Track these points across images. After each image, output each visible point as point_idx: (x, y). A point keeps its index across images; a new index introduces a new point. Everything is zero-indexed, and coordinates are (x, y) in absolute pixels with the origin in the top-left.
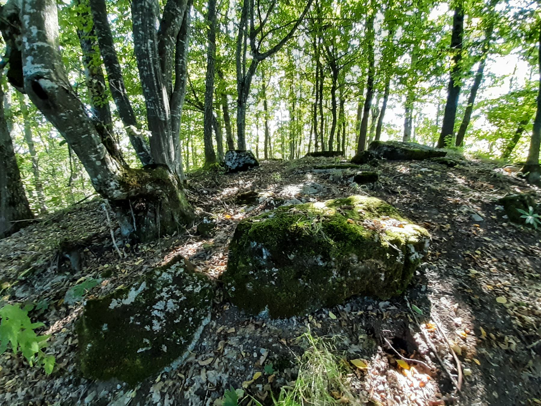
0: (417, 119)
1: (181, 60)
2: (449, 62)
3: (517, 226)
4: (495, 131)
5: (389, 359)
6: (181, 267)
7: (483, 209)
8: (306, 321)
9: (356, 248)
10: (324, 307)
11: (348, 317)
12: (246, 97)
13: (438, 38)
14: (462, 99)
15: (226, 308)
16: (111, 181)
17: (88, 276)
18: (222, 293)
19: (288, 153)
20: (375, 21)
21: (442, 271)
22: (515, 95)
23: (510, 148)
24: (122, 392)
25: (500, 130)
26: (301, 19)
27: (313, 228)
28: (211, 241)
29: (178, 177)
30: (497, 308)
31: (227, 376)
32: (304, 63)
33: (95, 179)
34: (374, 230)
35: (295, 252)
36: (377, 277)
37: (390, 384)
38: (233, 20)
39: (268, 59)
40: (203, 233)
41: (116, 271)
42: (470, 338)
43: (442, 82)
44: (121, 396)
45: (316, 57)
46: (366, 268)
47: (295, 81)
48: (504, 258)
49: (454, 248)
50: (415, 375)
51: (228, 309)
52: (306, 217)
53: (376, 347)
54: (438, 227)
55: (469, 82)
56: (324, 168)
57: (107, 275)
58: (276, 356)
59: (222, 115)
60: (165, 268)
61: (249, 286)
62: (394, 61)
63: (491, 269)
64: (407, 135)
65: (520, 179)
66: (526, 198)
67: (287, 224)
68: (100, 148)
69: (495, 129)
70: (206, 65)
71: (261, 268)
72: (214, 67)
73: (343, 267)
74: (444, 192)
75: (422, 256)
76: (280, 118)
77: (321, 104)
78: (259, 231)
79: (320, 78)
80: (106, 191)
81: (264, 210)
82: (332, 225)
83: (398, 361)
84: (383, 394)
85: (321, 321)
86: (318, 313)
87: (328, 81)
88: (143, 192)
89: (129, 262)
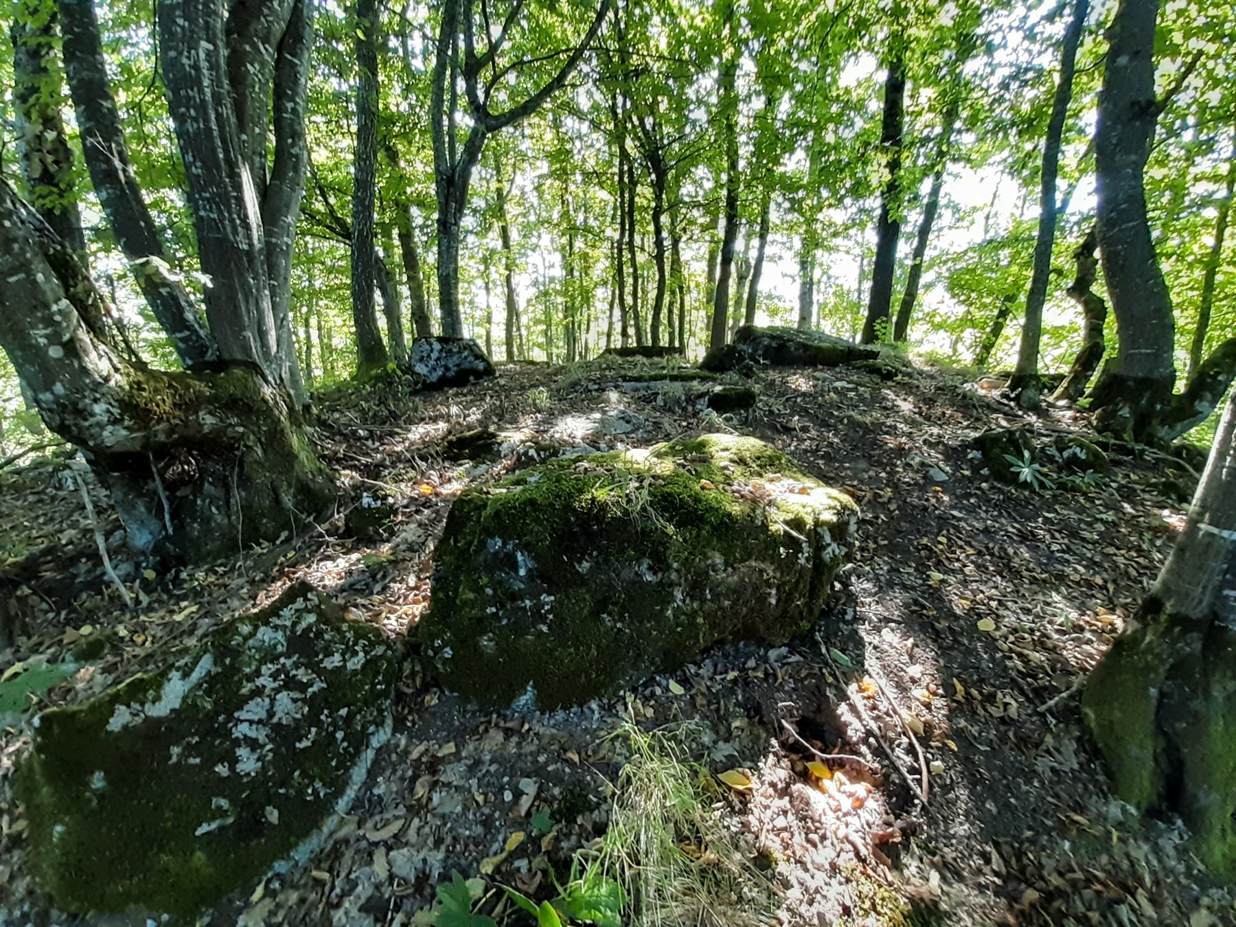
0: (822, 286)
1: (290, 105)
2: (877, 173)
4: (960, 315)
5: (793, 763)
7: (947, 459)
8: (620, 707)
9: (719, 539)
10: (658, 672)
11: (708, 688)
12: (460, 211)
13: (859, 123)
14: (903, 249)
15: (432, 700)
16: (96, 401)
17: (33, 659)
18: (417, 668)
19: (560, 349)
20: (738, 72)
22: (993, 245)
23: (987, 348)
25: (969, 312)
26: (584, 46)
27: (629, 501)
28: (386, 548)
29: (289, 395)
31: (441, 855)
32: (592, 149)
35: (591, 555)
36: (763, 598)
37: (797, 813)
38: (422, 27)
39: (507, 130)
40: (365, 527)
41: (116, 644)
42: (938, 702)
43: (868, 212)
45: (617, 137)
46: (742, 580)
47: (572, 188)
48: (987, 548)
49: (899, 533)
51: (435, 701)
52: (613, 478)
53: (767, 741)
54: (869, 495)
55: (914, 217)
57: (89, 653)
58: (556, 791)
59: (398, 251)
60: (264, 618)
61: (486, 642)
62: (776, 161)
63: (967, 570)
64: (804, 318)
67: (570, 495)
68: (60, 312)
69: (961, 310)
70: (354, 129)
71: (515, 597)
72: (375, 136)
73: (695, 581)
74: (877, 427)
75: (844, 550)
76: (541, 271)
77: (631, 243)
78: (507, 514)
79: (627, 186)
80: (80, 428)
81: (513, 471)
82: (670, 494)
83: (809, 764)
84: (785, 835)
86: (645, 685)
87: (644, 194)
88: (192, 432)
89: (155, 617)
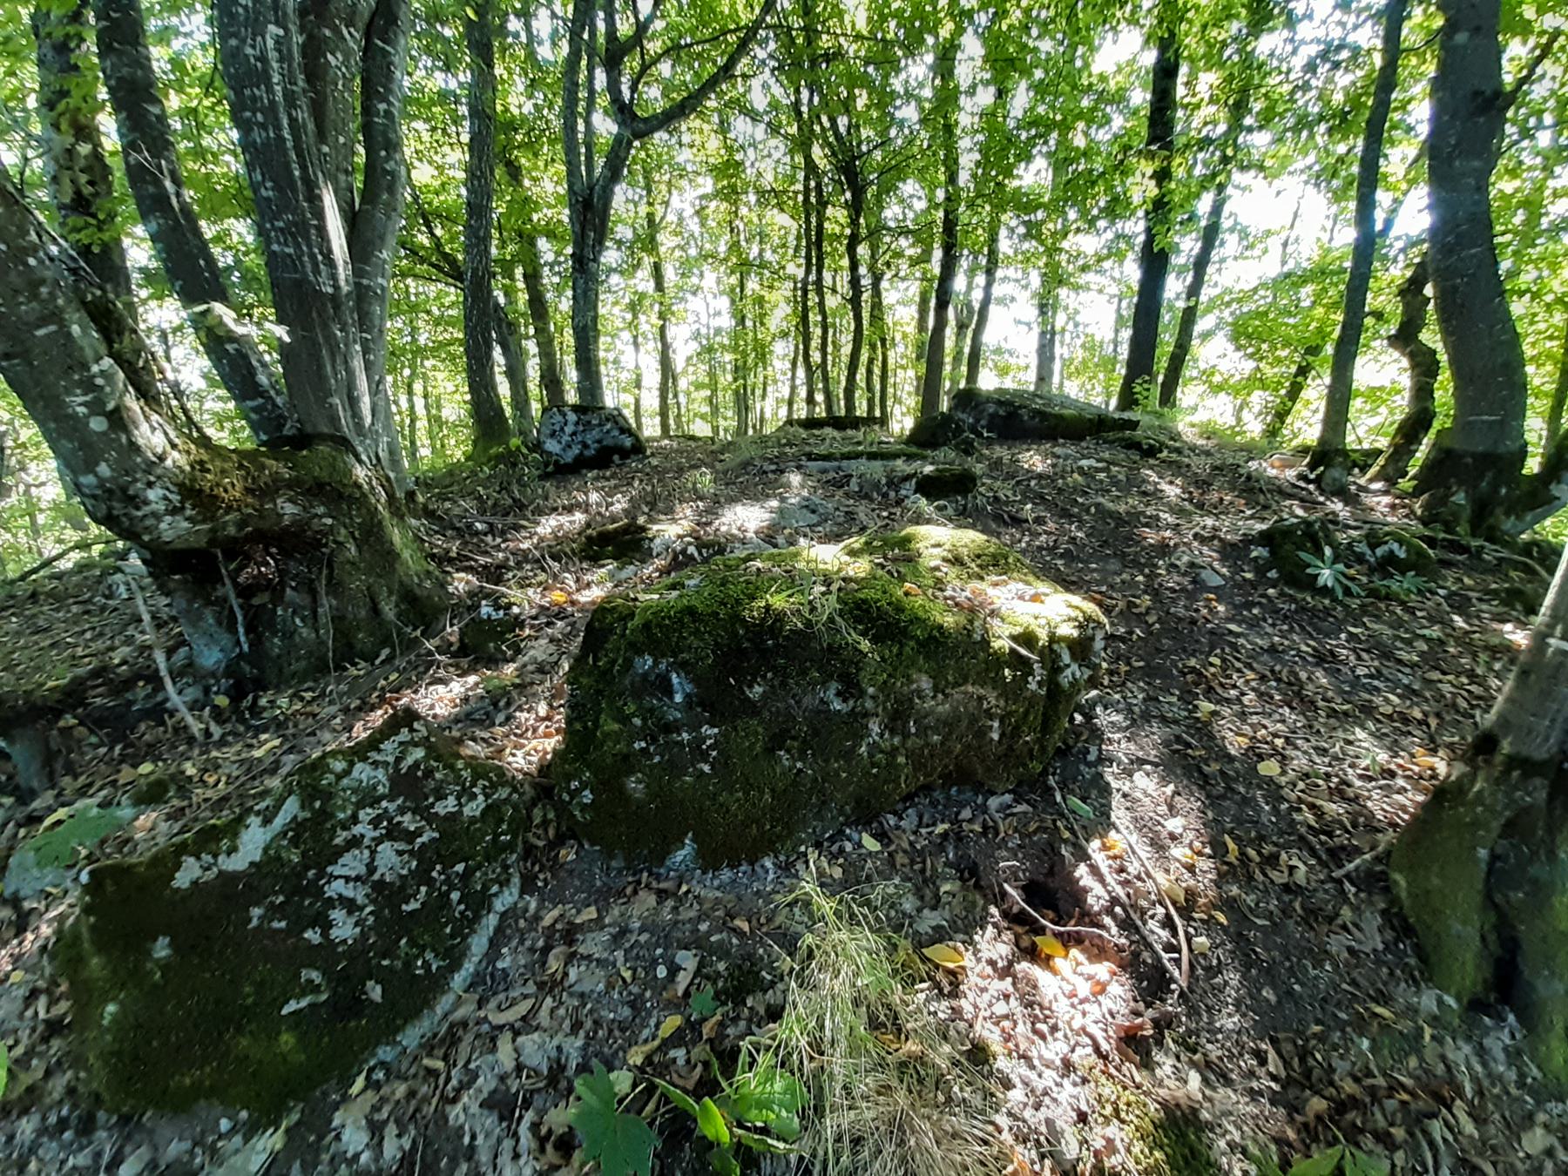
0: (1067, 336)
1: (382, 107)
2: (1140, 187)
3: (1300, 596)
4: (1247, 374)
5: (1017, 937)
6: (416, 745)
7: (1224, 559)
9: (927, 658)
11: (911, 844)
13: (1118, 122)
14: (1174, 287)
15: (568, 855)
16: (150, 485)
18: (551, 815)
19: (728, 421)
21: (1136, 709)
22: (1291, 280)
24: (238, 1139)
25: (1258, 369)
27: (813, 609)
28: (510, 669)
30: (1261, 788)
32: (770, 160)
33: (88, 480)
34: (972, 610)
36: (982, 733)
37: (1021, 998)
39: (660, 136)
40: (484, 643)
41: (183, 785)
44: (237, 1151)
45: (802, 144)
47: (744, 211)
48: (1272, 671)
49: (1159, 651)
50: (1079, 969)
51: (572, 857)
52: (792, 581)
53: (985, 909)
55: (1188, 245)
56: (831, 454)
57: (151, 795)
58: (721, 966)
59: (523, 297)
60: (360, 752)
61: (634, 785)
62: (1008, 172)
63: (1245, 700)
64: (1043, 377)
65: (1303, 485)
66: (1317, 526)
70: (465, 138)
74: (1134, 518)
75: (1088, 673)
76: (704, 320)
79: (813, 207)
80: (131, 519)
82: (864, 601)
83: (1038, 939)
84: (1006, 1024)
85: (841, 861)
86: (832, 840)
87: (837, 217)
89: (230, 752)
